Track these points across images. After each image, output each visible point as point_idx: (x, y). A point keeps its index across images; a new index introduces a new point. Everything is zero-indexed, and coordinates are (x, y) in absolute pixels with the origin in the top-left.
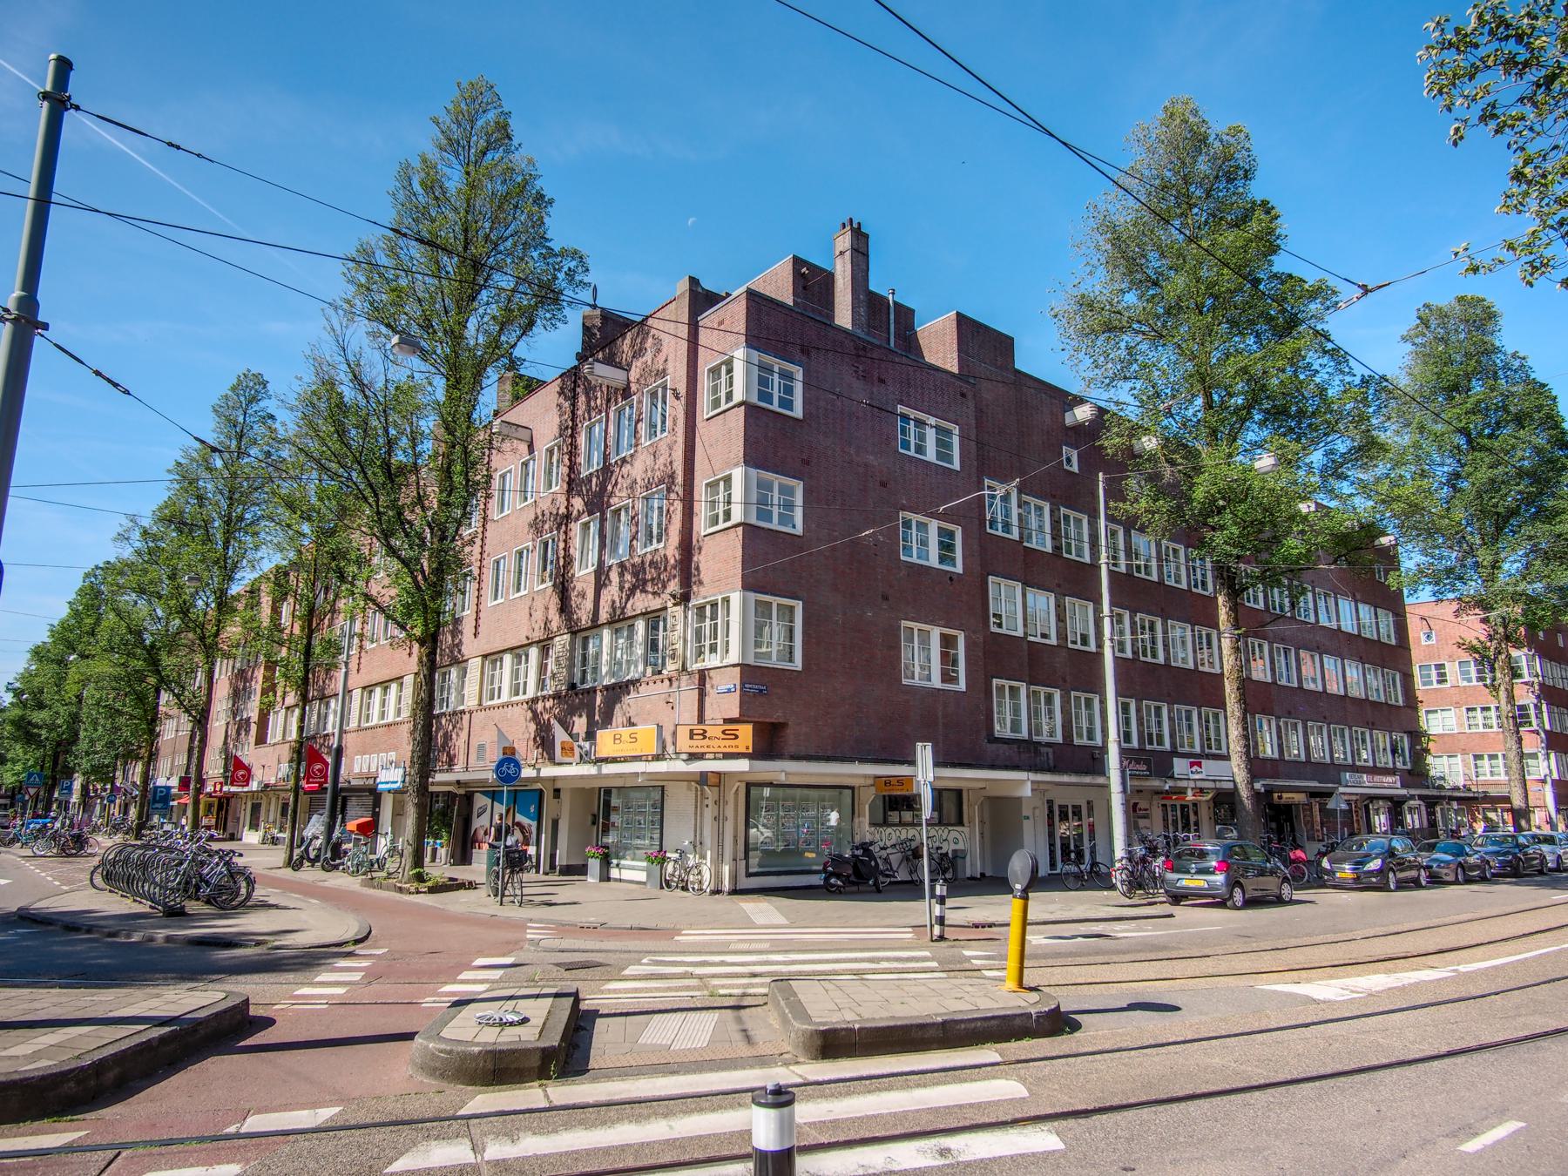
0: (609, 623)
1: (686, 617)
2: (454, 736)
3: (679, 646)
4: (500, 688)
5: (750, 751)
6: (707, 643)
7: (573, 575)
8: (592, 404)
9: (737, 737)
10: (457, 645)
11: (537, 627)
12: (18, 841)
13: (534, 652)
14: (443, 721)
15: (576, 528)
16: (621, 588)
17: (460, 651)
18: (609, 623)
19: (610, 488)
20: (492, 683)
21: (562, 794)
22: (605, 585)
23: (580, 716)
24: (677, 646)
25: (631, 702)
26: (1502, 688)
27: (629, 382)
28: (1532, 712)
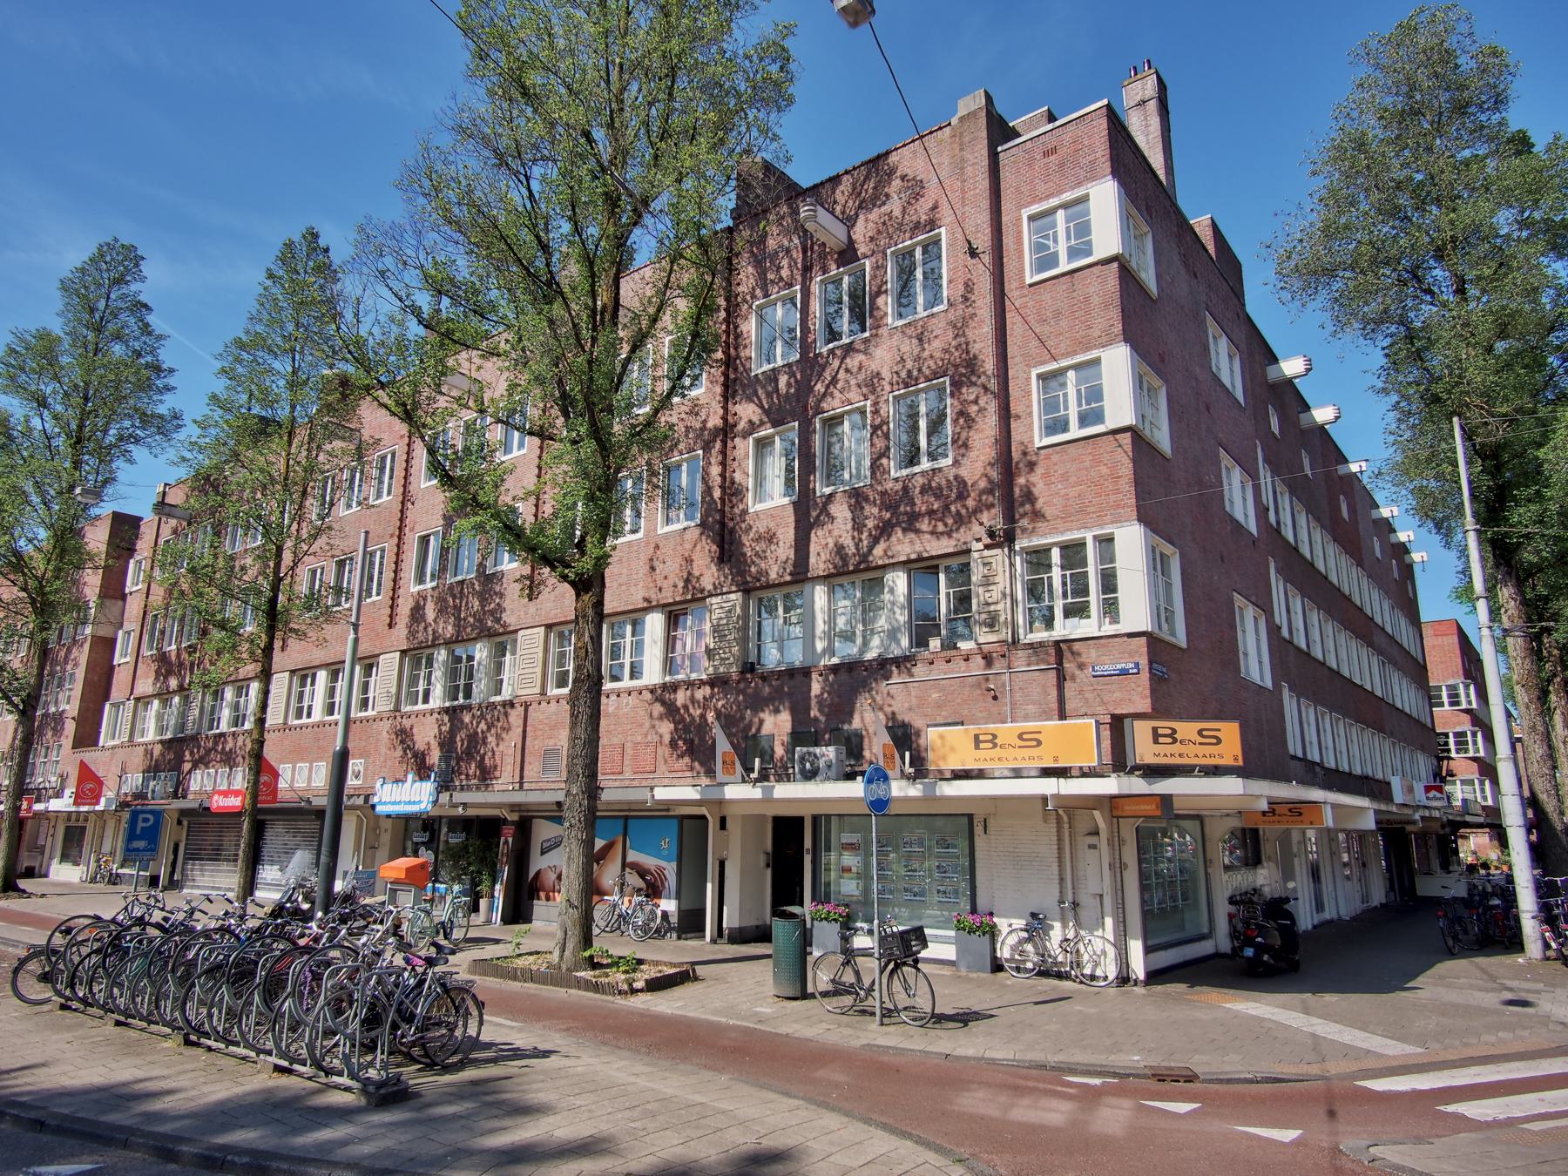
0: (825, 578)
1: (1012, 565)
2: (491, 739)
3: (1003, 607)
4: (310, 707)
5: (1241, 763)
6: (627, 661)
7: (745, 512)
8: (771, 276)
9: (1219, 741)
10: (492, 612)
11: (666, 585)
12: (589, 132)
13: (322, 676)
14: (467, 719)
15: (744, 448)
16: (858, 526)
17: (498, 620)
18: (825, 578)
19: (820, 388)
20: (561, 665)
21: (729, 824)
22: (818, 523)
23: (777, 711)
24: (1000, 607)
25: (893, 689)
26: (1558, 711)
27: (851, 242)
28: (1469, 738)
